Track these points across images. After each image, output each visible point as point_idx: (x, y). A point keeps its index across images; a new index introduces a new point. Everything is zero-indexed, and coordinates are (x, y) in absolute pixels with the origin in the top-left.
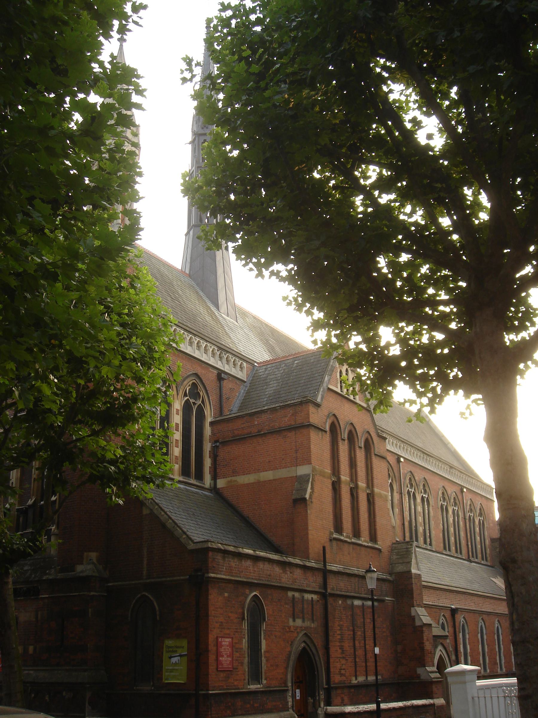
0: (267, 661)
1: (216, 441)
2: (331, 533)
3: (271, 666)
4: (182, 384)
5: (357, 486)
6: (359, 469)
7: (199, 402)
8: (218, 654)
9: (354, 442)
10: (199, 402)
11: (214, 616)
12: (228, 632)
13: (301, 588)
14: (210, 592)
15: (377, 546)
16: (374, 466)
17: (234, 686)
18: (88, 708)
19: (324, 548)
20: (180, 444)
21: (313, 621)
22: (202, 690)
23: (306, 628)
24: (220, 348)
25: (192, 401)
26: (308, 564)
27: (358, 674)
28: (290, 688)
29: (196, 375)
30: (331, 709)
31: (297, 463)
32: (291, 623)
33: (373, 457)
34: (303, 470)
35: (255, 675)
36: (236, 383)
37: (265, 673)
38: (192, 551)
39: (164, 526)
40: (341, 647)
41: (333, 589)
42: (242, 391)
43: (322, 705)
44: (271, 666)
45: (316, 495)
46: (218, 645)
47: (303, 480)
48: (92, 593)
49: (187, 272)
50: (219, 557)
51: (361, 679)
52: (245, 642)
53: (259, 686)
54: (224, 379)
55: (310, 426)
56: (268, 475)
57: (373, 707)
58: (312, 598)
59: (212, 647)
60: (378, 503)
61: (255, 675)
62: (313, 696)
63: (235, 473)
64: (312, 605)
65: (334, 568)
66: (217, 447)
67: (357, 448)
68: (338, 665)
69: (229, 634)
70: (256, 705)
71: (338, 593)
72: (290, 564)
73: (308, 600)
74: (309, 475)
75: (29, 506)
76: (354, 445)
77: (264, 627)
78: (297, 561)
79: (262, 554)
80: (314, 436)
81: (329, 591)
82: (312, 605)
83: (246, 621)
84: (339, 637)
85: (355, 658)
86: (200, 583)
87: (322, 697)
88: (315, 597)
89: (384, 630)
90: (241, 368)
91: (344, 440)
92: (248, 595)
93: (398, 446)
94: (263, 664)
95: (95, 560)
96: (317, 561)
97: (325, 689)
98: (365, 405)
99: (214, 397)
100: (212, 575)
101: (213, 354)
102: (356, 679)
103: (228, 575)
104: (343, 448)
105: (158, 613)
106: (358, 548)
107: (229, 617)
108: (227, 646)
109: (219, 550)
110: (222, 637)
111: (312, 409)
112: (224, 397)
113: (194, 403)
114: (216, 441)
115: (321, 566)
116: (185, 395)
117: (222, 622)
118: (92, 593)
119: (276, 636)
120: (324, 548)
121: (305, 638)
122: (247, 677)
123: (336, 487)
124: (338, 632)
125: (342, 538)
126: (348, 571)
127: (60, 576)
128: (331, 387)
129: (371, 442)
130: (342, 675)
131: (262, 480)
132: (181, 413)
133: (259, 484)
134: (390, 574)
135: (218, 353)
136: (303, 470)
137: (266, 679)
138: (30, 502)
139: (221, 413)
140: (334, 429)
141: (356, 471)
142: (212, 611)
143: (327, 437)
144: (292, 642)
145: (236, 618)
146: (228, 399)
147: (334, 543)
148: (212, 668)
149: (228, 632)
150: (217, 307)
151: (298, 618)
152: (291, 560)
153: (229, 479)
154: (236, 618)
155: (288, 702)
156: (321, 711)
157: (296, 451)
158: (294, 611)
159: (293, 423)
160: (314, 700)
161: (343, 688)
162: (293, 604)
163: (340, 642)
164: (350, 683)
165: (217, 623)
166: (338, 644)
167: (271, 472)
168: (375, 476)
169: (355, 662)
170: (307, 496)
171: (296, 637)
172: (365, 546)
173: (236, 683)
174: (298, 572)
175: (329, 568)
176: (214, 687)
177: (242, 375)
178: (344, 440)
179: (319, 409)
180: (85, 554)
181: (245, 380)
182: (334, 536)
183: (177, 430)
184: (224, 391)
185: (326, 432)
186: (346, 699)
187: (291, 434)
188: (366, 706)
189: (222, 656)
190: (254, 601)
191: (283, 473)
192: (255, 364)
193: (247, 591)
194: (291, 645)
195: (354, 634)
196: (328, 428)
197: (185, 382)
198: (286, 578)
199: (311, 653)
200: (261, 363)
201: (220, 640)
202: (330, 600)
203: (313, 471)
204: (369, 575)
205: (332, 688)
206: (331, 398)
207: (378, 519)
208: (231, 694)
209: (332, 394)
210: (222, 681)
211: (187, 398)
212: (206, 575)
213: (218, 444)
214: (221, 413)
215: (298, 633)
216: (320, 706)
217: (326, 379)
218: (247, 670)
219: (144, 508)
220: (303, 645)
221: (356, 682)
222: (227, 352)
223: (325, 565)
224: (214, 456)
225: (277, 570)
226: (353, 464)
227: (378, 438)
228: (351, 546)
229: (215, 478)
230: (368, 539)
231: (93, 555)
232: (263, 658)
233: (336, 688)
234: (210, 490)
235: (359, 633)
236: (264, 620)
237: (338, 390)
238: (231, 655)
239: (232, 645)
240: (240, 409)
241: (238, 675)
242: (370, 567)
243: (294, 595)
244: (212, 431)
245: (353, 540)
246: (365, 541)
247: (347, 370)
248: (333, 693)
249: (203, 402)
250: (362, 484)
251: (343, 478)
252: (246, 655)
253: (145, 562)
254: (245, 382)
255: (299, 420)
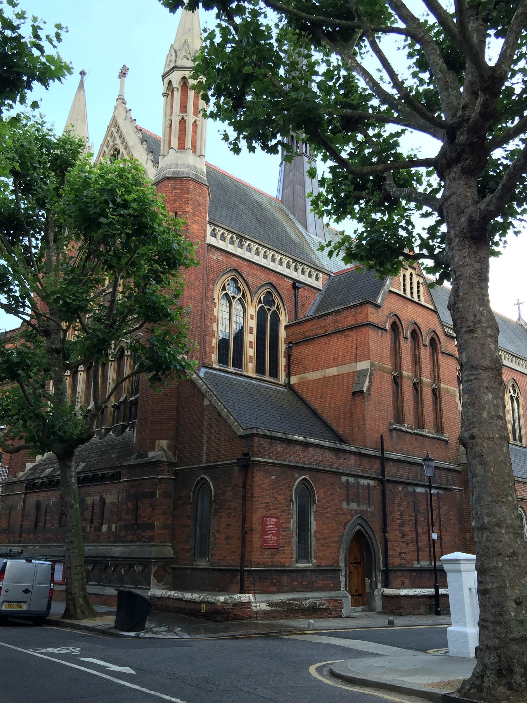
0: (317, 541)
1: (290, 343)
2: (391, 424)
3: (322, 546)
4: (256, 293)
5: (421, 381)
6: (423, 366)
7: (274, 308)
8: (264, 533)
9: (418, 340)
10: (274, 308)
11: (259, 497)
12: (274, 512)
13: (356, 473)
14: (255, 474)
15: (443, 438)
16: (441, 363)
17: (281, 563)
18: (153, 581)
19: (382, 437)
20: (255, 345)
21: (369, 504)
22: (247, 566)
23: (362, 512)
24: (295, 261)
25: (266, 307)
26: (364, 451)
27: (420, 558)
28: (343, 568)
29: (271, 284)
30: (388, 591)
31: (357, 359)
32: (345, 505)
33: (440, 354)
34: (363, 365)
35: (304, 553)
36: (312, 291)
37: (315, 553)
38: (242, 437)
39: (220, 415)
40: (402, 532)
41: (392, 476)
42: (318, 298)
43: (379, 586)
44: (322, 546)
45: (374, 388)
46: (264, 524)
47: (362, 374)
48: (160, 477)
49: (280, 199)
50: (265, 443)
51: (424, 563)
52: (293, 523)
53: (308, 565)
54: (299, 288)
55: (370, 325)
56: (332, 371)
57: (430, 591)
58: (368, 483)
59: (257, 527)
60: (445, 398)
61: (304, 553)
62: (370, 578)
63: (305, 370)
64: (369, 490)
65: (393, 457)
66: (291, 347)
67: (422, 346)
68: (398, 549)
69: (276, 514)
70: (304, 583)
71: (398, 479)
72: (344, 451)
73: (363, 485)
74: (367, 370)
75: (121, 402)
76: (418, 345)
77: (314, 508)
78: (353, 449)
79: (313, 441)
80: (372, 333)
81: (387, 477)
82: (369, 490)
83: (295, 503)
84: (398, 521)
85: (417, 543)
86: (246, 465)
87: (380, 578)
88: (372, 483)
89: (451, 517)
90: (317, 279)
91: (426, 346)
92: (297, 478)
93: (510, 360)
94: (313, 544)
95: (165, 448)
96: (374, 449)
97: (382, 571)
98: (432, 307)
99: (289, 304)
100: (257, 459)
101: (288, 266)
102: (418, 563)
103: (276, 459)
104: (406, 347)
105: (213, 494)
106: (422, 438)
107: (276, 498)
108: (273, 525)
109: (265, 436)
110: (267, 517)
111: (370, 309)
112: (299, 304)
113: (269, 310)
114: (290, 343)
115: (378, 454)
116: (260, 302)
117: (268, 503)
118: (160, 477)
119: (327, 518)
120: (382, 437)
121: (360, 521)
122: (294, 556)
123: (397, 381)
124: (398, 517)
125: (404, 429)
126: (409, 460)
127: (137, 461)
128: (392, 289)
129: (437, 341)
130: (402, 558)
131: (327, 376)
132: (255, 318)
133: (326, 380)
134: (459, 465)
135: (294, 265)
136: (363, 365)
137: (315, 558)
138: (122, 399)
139: (296, 317)
140: (395, 327)
141: (420, 367)
142: (257, 492)
143: (388, 337)
144: (345, 524)
145: (284, 499)
146: (303, 305)
147: (394, 433)
148: (257, 543)
149: (274, 512)
150: (306, 227)
151: (353, 502)
152: (346, 447)
153: (300, 376)
154: (284, 499)
155: (340, 582)
156: (378, 592)
157: (357, 348)
158: (348, 495)
159: (354, 323)
160: (371, 581)
161: (404, 571)
162: (348, 490)
163: (399, 526)
164: (412, 567)
165: (262, 503)
166: (398, 528)
167: (335, 368)
168: (441, 372)
169: (418, 546)
170: (365, 389)
171: (350, 520)
172: (429, 437)
173: (282, 561)
174: (353, 459)
175: (386, 455)
176: (258, 564)
177: (319, 284)
178: (407, 338)
179: (379, 310)
180: (157, 441)
181: (321, 289)
182: (394, 426)
183: (251, 333)
184: (299, 299)
185: (386, 330)
186: (407, 582)
187: (352, 333)
188: (164, 592)
189: (268, 535)
190: (304, 484)
191: (345, 369)
192: (332, 274)
193: (296, 475)
194: (344, 527)
195: (416, 521)
196: (388, 327)
197: (260, 291)
198: (340, 464)
199: (367, 536)
200: (336, 273)
201: (265, 519)
202: (389, 487)
203: (371, 366)
204: (427, 463)
205: (391, 570)
206: (393, 300)
207: (444, 412)
208: (277, 571)
209: (394, 296)
210: (267, 558)
211: (260, 305)
212: (252, 459)
213: (291, 345)
214: (296, 317)
215: (352, 516)
216: (376, 587)
217: (388, 282)
218: (295, 549)
219: (205, 399)
220: (358, 527)
221: (419, 566)
222: (303, 264)
223: (383, 453)
224: (288, 357)
225: (328, 454)
226: (416, 360)
227: (445, 337)
228: (414, 436)
229: (288, 376)
230: (432, 431)
231: (164, 443)
232: (313, 538)
233: (396, 571)
234: (284, 386)
235: (422, 519)
236: (315, 502)
237: (401, 293)
238: (277, 534)
239: (277, 525)
240: (317, 310)
241: (284, 553)
242: (428, 456)
243: (348, 480)
244: (287, 334)
245: (415, 431)
246: (429, 432)
247: (411, 274)
248: (391, 576)
249: (278, 308)
250: (426, 380)
251: (405, 373)
252: (294, 535)
253: (205, 448)
254: (320, 290)
255: (360, 320)
